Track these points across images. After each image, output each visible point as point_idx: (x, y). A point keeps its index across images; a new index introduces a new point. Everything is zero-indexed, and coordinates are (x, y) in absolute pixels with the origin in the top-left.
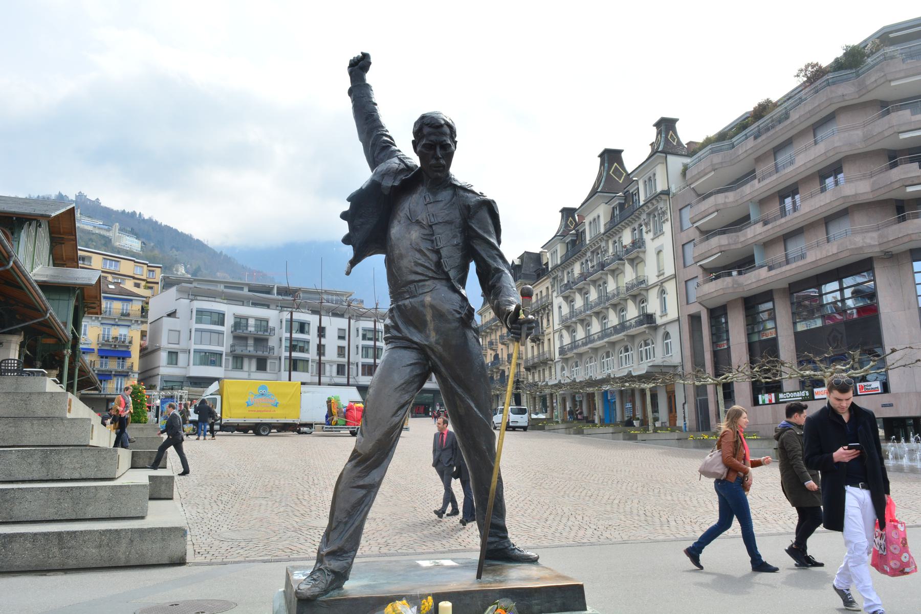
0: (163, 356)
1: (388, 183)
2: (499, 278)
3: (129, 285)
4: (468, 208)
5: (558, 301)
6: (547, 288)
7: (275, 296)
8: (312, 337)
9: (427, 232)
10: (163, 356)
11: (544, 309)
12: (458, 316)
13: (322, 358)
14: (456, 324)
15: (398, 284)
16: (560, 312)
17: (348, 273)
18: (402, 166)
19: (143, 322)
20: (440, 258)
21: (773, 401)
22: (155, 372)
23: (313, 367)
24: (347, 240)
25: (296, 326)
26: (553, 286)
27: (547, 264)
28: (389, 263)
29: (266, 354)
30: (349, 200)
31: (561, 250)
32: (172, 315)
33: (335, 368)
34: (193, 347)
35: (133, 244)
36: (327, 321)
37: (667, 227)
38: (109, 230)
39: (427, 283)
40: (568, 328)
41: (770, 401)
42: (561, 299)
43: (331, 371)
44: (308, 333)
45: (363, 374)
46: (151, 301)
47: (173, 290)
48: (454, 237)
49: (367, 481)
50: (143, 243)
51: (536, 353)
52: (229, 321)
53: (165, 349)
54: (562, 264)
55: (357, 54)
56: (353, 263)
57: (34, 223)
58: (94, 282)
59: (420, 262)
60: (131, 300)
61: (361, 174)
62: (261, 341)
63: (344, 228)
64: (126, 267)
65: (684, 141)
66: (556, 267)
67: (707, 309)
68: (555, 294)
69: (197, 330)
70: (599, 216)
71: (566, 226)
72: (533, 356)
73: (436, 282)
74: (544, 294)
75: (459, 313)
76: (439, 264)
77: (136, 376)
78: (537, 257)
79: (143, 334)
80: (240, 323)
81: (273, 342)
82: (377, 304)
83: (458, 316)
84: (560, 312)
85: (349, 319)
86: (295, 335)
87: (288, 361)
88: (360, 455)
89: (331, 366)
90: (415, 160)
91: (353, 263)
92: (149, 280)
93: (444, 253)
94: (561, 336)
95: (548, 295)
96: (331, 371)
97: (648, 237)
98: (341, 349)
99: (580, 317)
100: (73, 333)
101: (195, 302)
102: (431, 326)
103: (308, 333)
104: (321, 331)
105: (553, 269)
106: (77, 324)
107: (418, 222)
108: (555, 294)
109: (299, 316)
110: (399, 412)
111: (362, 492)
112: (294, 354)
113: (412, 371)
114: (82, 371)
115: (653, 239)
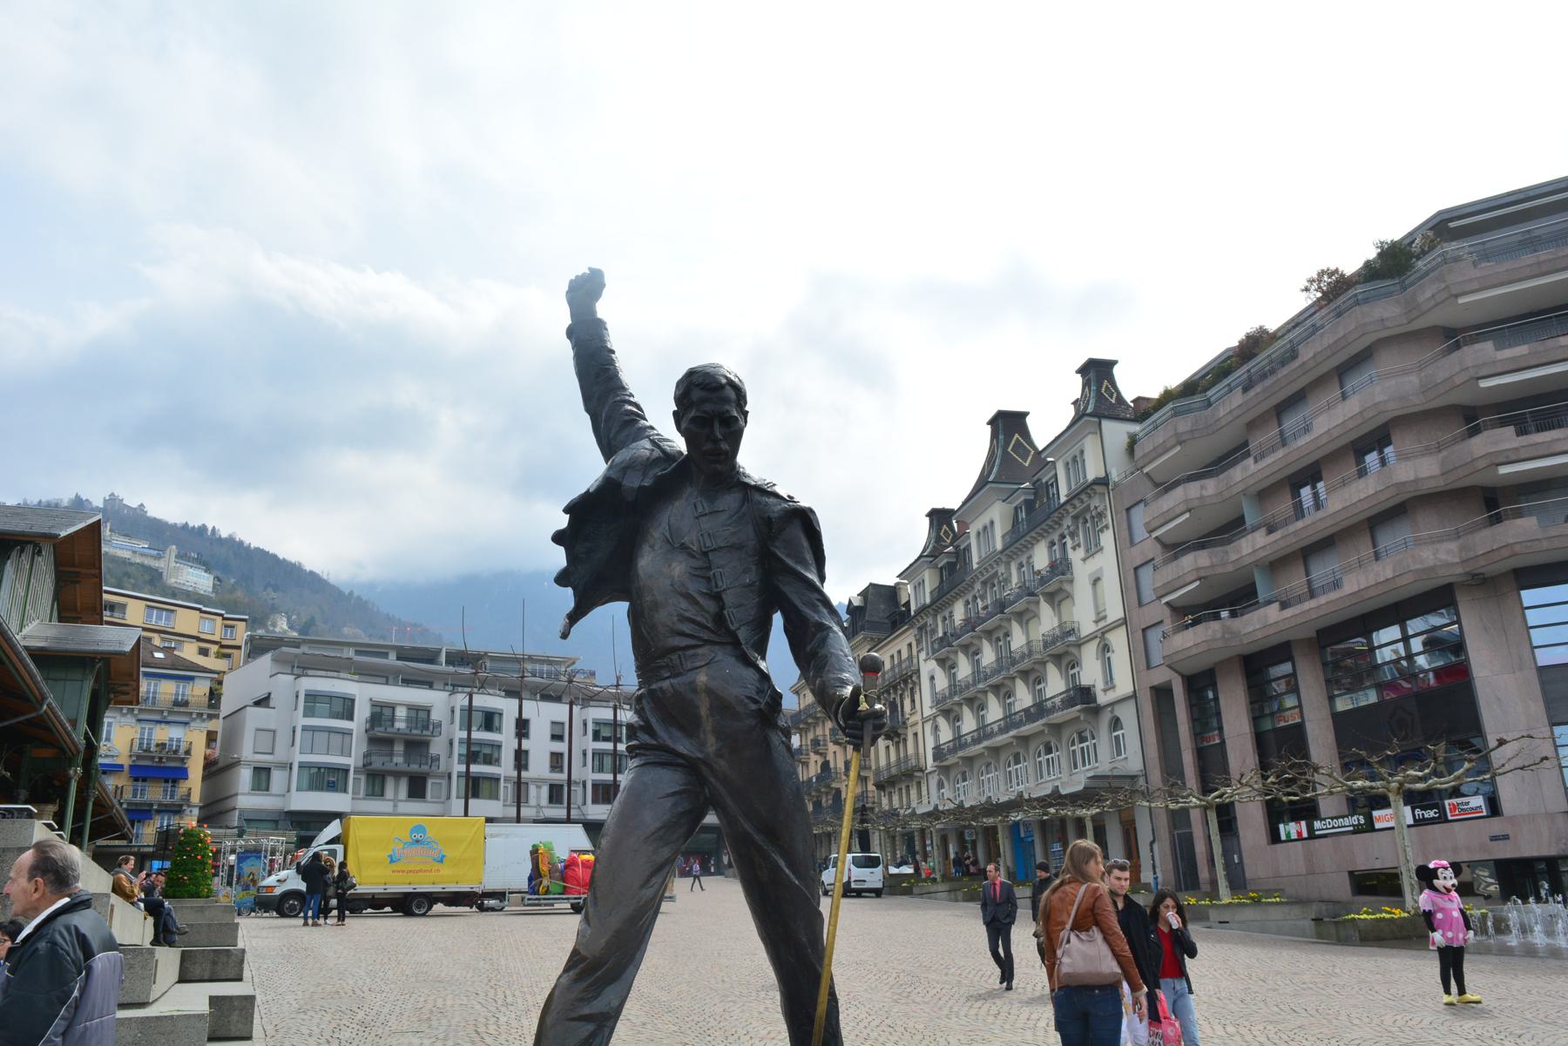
0: (245, 776)
1: (633, 482)
2: (824, 640)
3: (189, 652)
4: (769, 522)
5: (928, 667)
6: (910, 645)
7: (443, 667)
8: (506, 737)
9: (699, 564)
10: (245, 776)
11: (905, 682)
12: (753, 707)
13: (524, 774)
14: (751, 722)
15: (650, 651)
16: (933, 686)
17: (565, 636)
18: (657, 453)
19: (211, 717)
20: (722, 608)
21: (1305, 835)
22: (229, 804)
23: (506, 790)
24: (562, 579)
25: (478, 718)
26: (919, 642)
27: (908, 604)
28: (635, 617)
29: (425, 768)
30: (566, 511)
31: (930, 580)
32: (263, 702)
33: (545, 791)
34: (298, 758)
35: (199, 580)
36: (531, 708)
37: (1107, 539)
38: (158, 558)
39: (700, 651)
40: (946, 713)
41: (1300, 833)
42: (933, 664)
43: (538, 797)
44: (499, 730)
45: (595, 801)
46: (227, 679)
47: (266, 660)
48: (746, 571)
49: (597, 1006)
50: (217, 578)
51: (893, 758)
52: (362, 712)
53: (248, 763)
54: (933, 602)
55: (582, 270)
56: (574, 617)
57: (29, 548)
58: (128, 648)
59: (687, 614)
60: (192, 678)
61: (588, 467)
62: (417, 746)
63: (558, 558)
64: (186, 621)
65: (1129, 396)
66: (923, 610)
67: (1183, 676)
68: (923, 655)
69: (305, 728)
70: (992, 523)
71: (938, 539)
72: (889, 763)
73: (717, 648)
74: (905, 655)
75: (756, 702)
76: (719, 619)
77: (196, 811)
78: (891, 593)
79: (211, 737)
80: (381, 714)
81: (437, 747)
82: (618, 678)
83: (753, 707)
84: (933, 686)
85: (571, 704)
86: (476, 735)
87: (463, 781)
88: (584, 959)
89: (539, 787)
90: (680, 444)
91: (574, 617)
92: (224, 642)
93: (729, 598)
94: (936, 728)
95: (910, 657)
96: (538, 797)
97: (1076, 556)
98: (556, 760)
99: (967, 694)
100: (87, 737)
101: (303, 680)
102: (708, 725)
103: (499, 730)
104: (522, 727)
105: (918, 612)
106: (95, 722)
107: (684, 548)
108: (923, 655)
109: (484, 701)
110: (654, 880)
111: (591, 1027)
112: (474, 768)
113: (675, 805)
114: (101, 806)
115: (1084, 560)
